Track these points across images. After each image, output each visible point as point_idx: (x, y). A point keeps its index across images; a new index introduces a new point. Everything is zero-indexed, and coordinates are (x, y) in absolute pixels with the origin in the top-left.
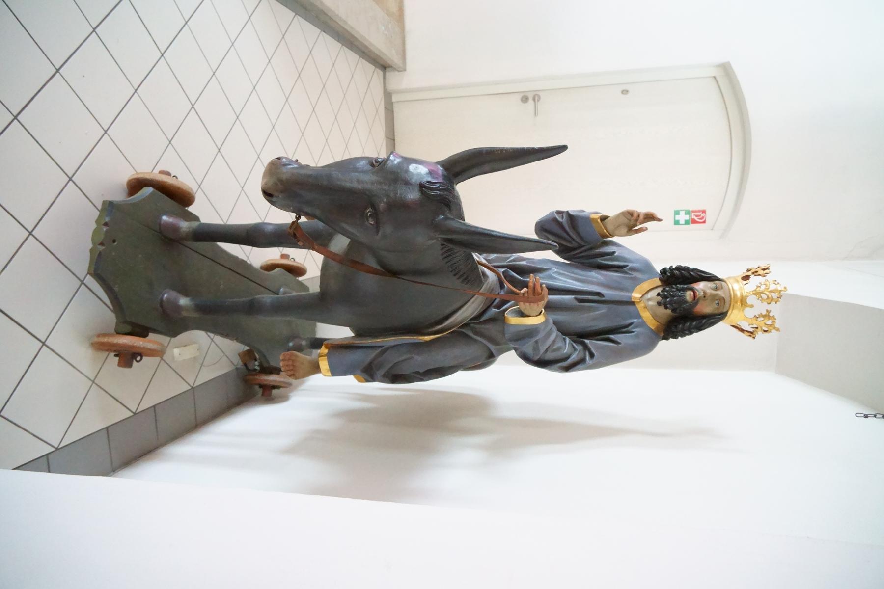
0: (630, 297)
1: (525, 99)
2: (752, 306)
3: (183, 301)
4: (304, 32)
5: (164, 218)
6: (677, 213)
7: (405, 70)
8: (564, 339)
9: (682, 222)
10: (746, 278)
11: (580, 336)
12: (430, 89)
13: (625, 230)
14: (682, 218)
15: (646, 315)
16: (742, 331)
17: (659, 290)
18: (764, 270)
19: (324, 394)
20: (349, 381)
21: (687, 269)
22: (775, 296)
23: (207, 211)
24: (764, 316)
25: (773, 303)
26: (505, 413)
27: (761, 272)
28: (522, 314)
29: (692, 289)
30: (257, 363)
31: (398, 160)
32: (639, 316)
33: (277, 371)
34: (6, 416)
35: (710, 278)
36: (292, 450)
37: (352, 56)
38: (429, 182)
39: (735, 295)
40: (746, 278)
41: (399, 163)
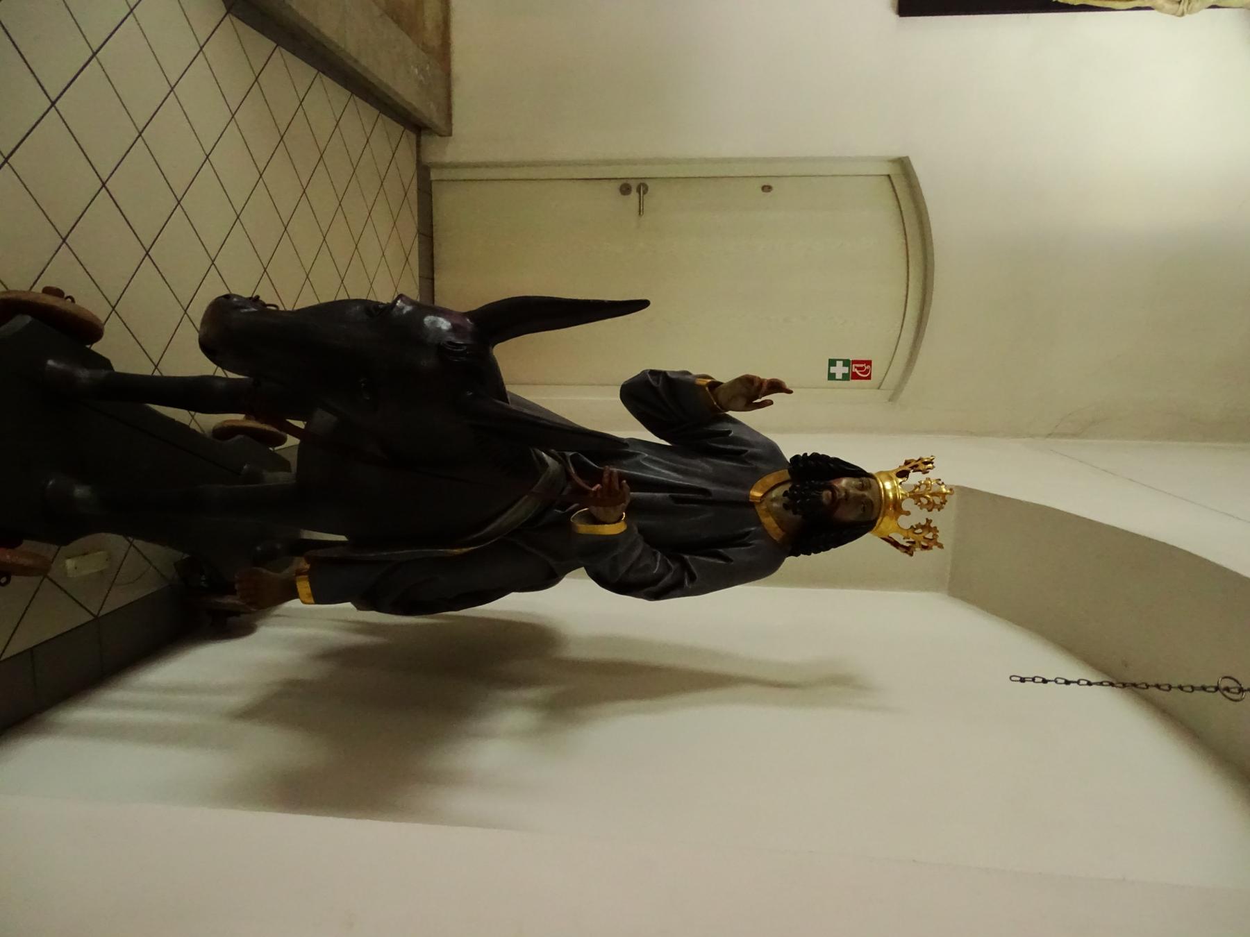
0: (748, 496)
1: (625, 190)
2: (908, 513)
3: (80, 491)
4: (288, 75)
5: (51, 363)
6: (832, 363)
7: (450, 134)
8: (655, 554)
9: (839, 376)
10: (903, 474)
11: (675, 549)
12: (486, 165)
13: (742, 402)
14: (840, 370)
15: (769, 522)
16: (896, 544)
17: (787, 487)
18: (926, 463)
19: (301, 631)
20: (347, 608)
21: (825, 458)
22: (937, 500)
23: (122, 353)
24: (923, 527)
25: (935, 510)
26: (574, 652)
27: (922, 467)
28: (596, 521)
29: (832, 489)
30: (203, 578)
31: (408, 308)
32: (760, 523)
33: (229, 590)
34: (10, 150)
35: (856, 472)
36: (250, 714)
37: (369, 112)
38: (450, 343)
39: (887, 496)
40: (903, 474)
41: (408, 313)
